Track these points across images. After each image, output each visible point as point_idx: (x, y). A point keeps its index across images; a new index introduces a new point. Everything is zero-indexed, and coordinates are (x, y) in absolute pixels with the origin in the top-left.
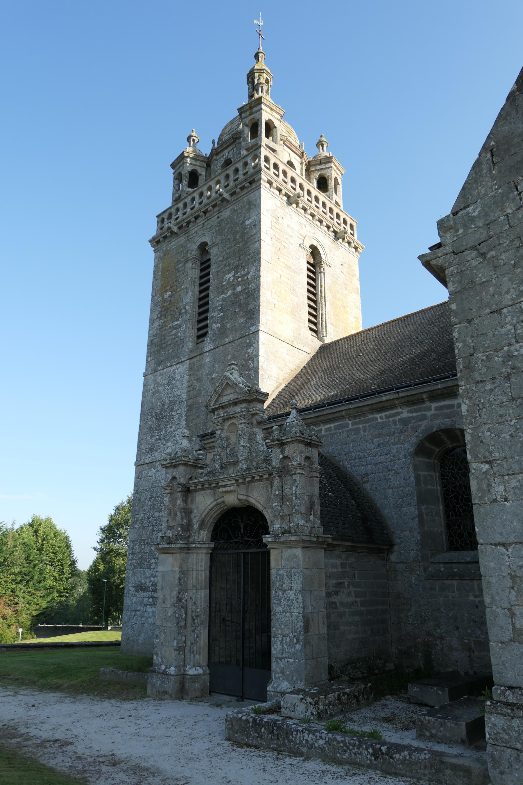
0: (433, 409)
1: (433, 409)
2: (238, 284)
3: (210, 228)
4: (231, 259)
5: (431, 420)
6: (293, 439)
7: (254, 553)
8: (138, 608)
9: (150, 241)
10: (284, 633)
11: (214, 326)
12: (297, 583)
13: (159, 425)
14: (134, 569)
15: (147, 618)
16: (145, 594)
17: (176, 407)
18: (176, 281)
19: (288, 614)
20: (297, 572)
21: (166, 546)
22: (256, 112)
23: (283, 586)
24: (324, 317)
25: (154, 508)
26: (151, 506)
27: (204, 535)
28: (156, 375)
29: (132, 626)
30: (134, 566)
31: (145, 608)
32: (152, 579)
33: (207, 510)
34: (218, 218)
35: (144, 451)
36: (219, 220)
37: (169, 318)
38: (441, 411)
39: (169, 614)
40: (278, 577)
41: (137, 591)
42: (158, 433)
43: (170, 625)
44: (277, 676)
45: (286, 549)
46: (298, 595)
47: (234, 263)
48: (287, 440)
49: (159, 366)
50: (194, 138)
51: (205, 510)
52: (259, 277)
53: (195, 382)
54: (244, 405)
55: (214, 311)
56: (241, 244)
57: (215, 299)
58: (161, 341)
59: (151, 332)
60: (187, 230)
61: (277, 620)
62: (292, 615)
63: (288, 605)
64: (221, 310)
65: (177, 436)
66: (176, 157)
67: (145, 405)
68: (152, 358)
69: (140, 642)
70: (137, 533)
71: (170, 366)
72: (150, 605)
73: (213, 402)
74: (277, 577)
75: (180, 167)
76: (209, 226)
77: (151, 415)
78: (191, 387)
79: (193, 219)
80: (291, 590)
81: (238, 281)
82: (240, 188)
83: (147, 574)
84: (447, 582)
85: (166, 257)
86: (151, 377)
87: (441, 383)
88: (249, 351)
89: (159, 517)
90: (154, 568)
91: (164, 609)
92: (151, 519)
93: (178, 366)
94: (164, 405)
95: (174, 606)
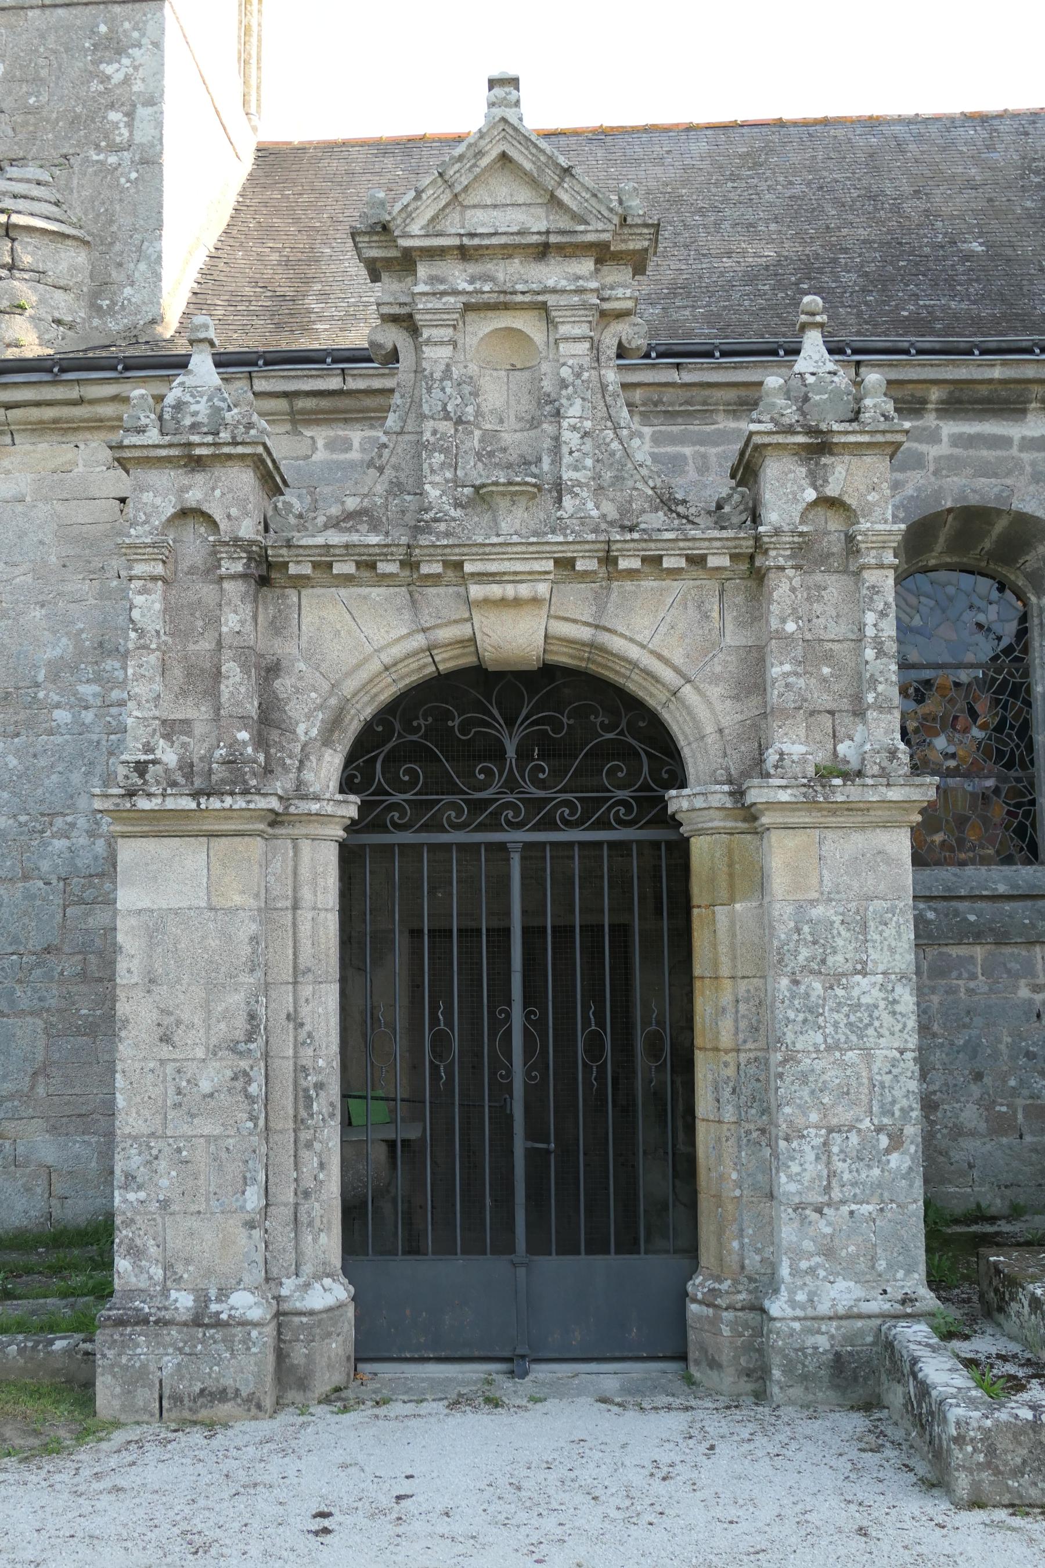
0: (945, 439)
1: (945, 439)
5: (935, 473)
6: (880, 438)
7: (570, 845)
10: (835, 1121)
12: (892, 950)
19: (851, 1056)
20: (892, 910)
23: (830, 960)
24: (254, 40)
27: (327, 768)
33: (375, 666)
38: (972, 452)
39: (206, 1086)
40: (806, 929)
44: (804, 1265)
45: (840, 833)
46: (899, 989)
48: (852, 439)
51: (358, 666)
54: (587, 266)
61: (804, 1078)
62: (868, 1056)
63: (849, 1025)
73: (423, 221)
74: (798, 931)
80: (864, 973)
84: (954, 951)
87: (1004, 363)
88: (109, 69)
91: (170, 1068)
95: (233, 1050)
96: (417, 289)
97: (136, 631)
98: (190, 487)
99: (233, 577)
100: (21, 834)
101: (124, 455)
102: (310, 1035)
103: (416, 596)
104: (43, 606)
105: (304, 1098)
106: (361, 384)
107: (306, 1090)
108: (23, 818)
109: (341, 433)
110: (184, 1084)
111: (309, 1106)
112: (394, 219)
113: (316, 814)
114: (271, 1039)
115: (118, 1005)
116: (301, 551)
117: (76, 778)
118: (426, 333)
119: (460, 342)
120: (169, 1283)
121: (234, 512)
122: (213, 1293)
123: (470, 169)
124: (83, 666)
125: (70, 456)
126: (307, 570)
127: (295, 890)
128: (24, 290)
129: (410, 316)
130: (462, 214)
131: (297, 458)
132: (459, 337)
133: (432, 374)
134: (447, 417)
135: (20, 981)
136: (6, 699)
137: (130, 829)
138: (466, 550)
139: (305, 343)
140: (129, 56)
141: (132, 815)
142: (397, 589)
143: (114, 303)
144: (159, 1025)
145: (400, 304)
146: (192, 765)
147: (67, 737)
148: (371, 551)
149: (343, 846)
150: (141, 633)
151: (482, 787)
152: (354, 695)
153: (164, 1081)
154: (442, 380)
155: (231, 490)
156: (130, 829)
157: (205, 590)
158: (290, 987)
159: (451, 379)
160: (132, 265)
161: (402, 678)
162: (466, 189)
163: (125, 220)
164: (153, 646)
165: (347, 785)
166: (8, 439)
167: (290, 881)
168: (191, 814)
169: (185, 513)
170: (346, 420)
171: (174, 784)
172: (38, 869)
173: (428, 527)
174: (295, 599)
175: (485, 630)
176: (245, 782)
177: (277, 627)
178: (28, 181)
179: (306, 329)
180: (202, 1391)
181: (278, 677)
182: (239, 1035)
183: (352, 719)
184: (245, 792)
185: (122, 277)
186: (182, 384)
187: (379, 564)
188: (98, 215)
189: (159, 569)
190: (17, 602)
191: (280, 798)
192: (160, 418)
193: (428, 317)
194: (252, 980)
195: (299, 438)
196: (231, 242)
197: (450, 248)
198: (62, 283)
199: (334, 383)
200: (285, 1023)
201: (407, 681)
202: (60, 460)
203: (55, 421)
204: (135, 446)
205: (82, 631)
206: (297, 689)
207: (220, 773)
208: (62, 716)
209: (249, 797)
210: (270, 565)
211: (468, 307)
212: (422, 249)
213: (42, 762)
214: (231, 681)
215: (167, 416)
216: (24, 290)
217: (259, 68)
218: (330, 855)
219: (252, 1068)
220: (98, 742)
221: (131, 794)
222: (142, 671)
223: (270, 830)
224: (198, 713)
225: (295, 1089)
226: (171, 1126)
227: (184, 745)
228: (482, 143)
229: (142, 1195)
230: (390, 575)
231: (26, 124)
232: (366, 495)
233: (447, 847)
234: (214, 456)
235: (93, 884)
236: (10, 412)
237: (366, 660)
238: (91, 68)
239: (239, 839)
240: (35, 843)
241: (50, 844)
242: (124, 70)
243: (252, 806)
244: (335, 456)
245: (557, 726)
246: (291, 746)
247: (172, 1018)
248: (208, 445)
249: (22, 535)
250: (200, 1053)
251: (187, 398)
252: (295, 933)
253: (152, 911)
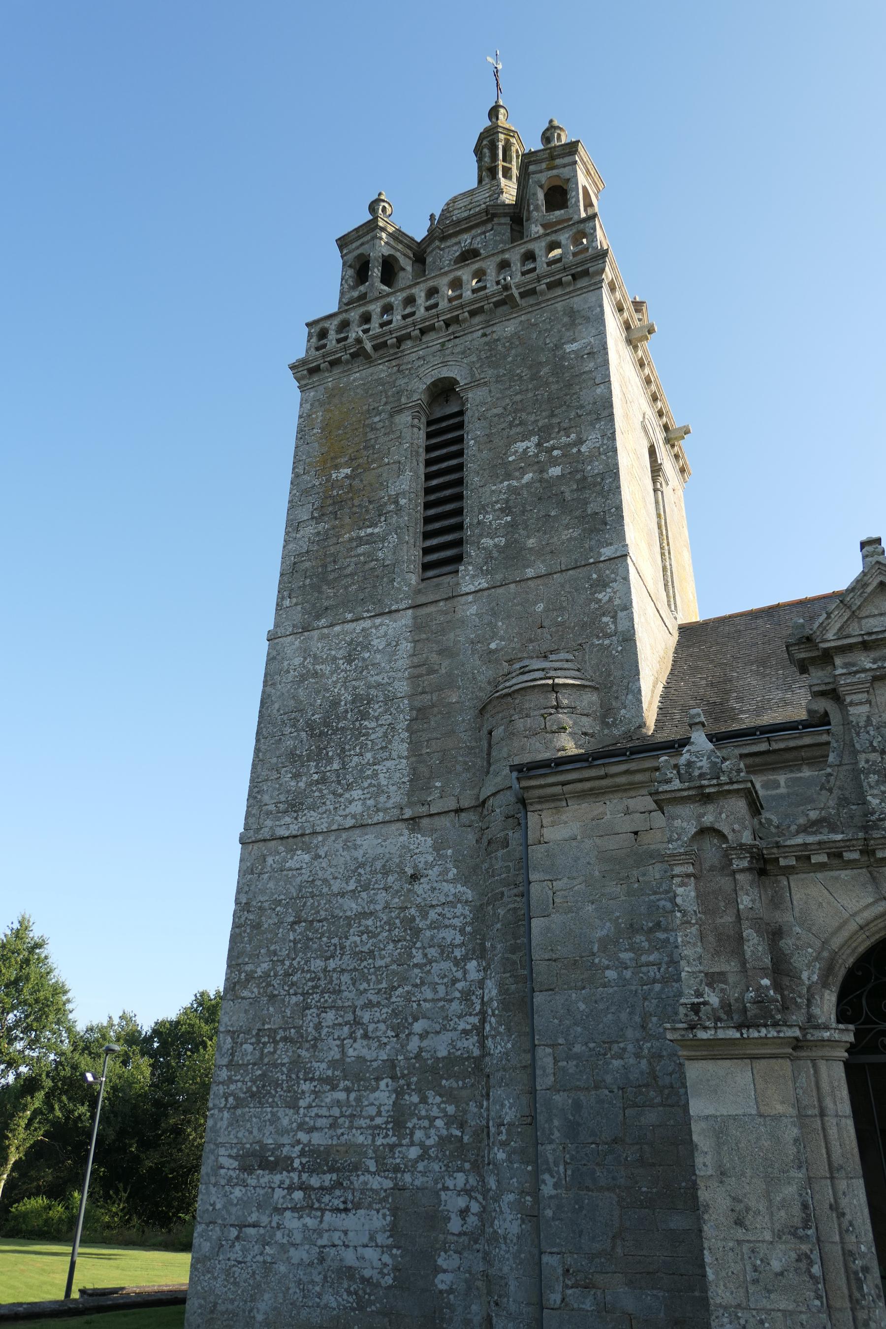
2: (554, 462)
3: (463, 353)
4: (528, 414)
8: (253, 1218)
9: (292, 367)
11: (487, 542)
13: (320, 750)
14: (235, 1108)
15: (283, 1248)
16: (277, 1178)
17: (376, 709)
18: (366, 448)
21: (734, 1034)
22: (564, 166)
24: (669, 573)
25: (307, 947)
26: (295, 942)
27: (827, 1005)
28: (310, 638)
29: (228, 1272)
30: (237, 1098)
31: (276, 1219)
32: (302, 1136)
33: (853, 926)
34: (484, 335)
35: (272, 808)
36: (485, 339)
37: (347, 520)
41: (246, 1168)
42: (316, 767)
43: (784, 1304)
47: (536, 421)
49: (318, 617)
50: (387, 205)
51: (840, 928)
52: (615, 450)
53: (434, 658)
55: (483, 509)
56: (554, 387)
57: (486, 488)
58: (324, 566)
59: (291, 546)
60: (396, 353)
64: (506, 510)
65: (381, 776)
66: (356, 226)
67: (273, 702)
68: (294, 600)
69: (260, 1317)
70: (246, 1011)
71: (352, 621)
72: (294, 1209)
75: (362, 244)
76: (457, 350)
77: (294, 726)
78: (420, 670)
79: (417, 332)
81: (551, 457)
82: (547, 284)
83: (285, 1122)
85: (336, 401)
86: (292, 645)
88: (600, 596)
89: (325, 970)
90: (310, 1106)
91: (745, 1248)
92: (299, 975)
93: (378, 621)
94: (335, 704)
95: (794, 1235)
96: (839, 671)
97: (680, 912)
98: (705, 814)
99: (742, 871)
100: (591, 1056)
101: (660, 798)
102: (851, 1224)
103: (875, 874)
104: (593, 903)
105: (855, 1280)
106: (782, 745)
107: (856, 1273)
108: (592, 1045)
109: (771, 777)
110: (758, 1262)
111: (860, 1289)
112: (815, 632)
113: (828, 1040)
114: (819, 1225)
115: (699, 1192)
116: (787, 849)
117: (624, 1016)
118: (848, 699)
119: (873, 701)
121: (736, 827)
123: (860, 595)
124: (621, 940)
125: (601, 809)
126: (793, 862)
127: (820, 1100)
128: (565, 719)
129: (834, 690)
130: (859, 622)
132: (872, 697)
133: (858, 724)
134: (874, 750)
135: (598, 1164)
136: (575, 964)
137: (693, 1053)
139: (735, 727)
140: (610, 587)
141: (694, 1043)
142: (860, 871)
143: (615, 720)
144: (732, 1210)
145: (826, 684)
146: (730, 1005)
147: (615, 988)
148: (838, 845)
149: (847, 1065)
150: (684, 913)
152: (840, 949)
153: (742, 1259)
154: (866, 727)
155: (732, 813)
156: (693, 1053)
157: (723, 881)
158: (829, 1181)
159: (872, 725)
160: (624, 697)
161: (873, 934)
162: (859, 607)
163: (618, 673)
164: (693, 921)
165: (842, 1018)
166: (564, 804)
167: (814, 1093)
168: (736, 1042)
169: (704, 832)
170: (774, 769)
171: (719, 1019)
172: (604, 1081)
173: (876, 825)
174: (786, 883)
176: (772, 1017)
177: (776, 903)
178: (562, 661)
179: (734, 719)
181: (782, 938)
182: (797, 1221)
183: (840, 967)
184: (775, 1024)
185: (619, 704)
186: (688, 751)
187: (844, 854)
188: (602, 672)
189: (690, 869)
190: (577, 902)
191: (800, 1028)
192: (678, 772)
193: (848, 688)
194: (800, 1175)
196: (675, 678)
197: (855, 644)
198: (585, 712)
199: (763, 747)
200: (829, 1212)
201: (877, 936)
202: (596, 813)
203: (591, 789)
204: (666, 792)
205: (618, 917)
206: (797, 946)
207: (752, 1009)
208: (611, 974)
209: (778, 1028)
210: (766, 861)
211: (875, 679)
212: (836, 648)
213: (601, 1006)
214: (751, 943)
215: (682, 772)
216: (565, 719)
217: (673, 587)
218: (839, 1071)
219: (811, 1251)
220: (636, 991)
221: (692, 1027)
222: (688, 939)
223: (795, 1054)
224: (730, 967)
225: (846, 1271)
226: (752, 1299)
227: (722, 990)
228: (866, 578)
230: (855, 860)
231: (558, 631)
232: (822, 809)
234: (719, 793)
235: (675, 1098)
236: (565, 788)
237: (845, 922)
238: (590, 597)
239: (774, 1061)
240: (601, 1063)
241: (611, 1063)
242: (608, 595)
243: (782, 1035)
246: (799, 988)
247: (742, 1205)
248: (714, 785)
249: (576, 860)
250: (768, 1236)
251: (694, 759)
252: (825, 1136)
253: (716, 1117)
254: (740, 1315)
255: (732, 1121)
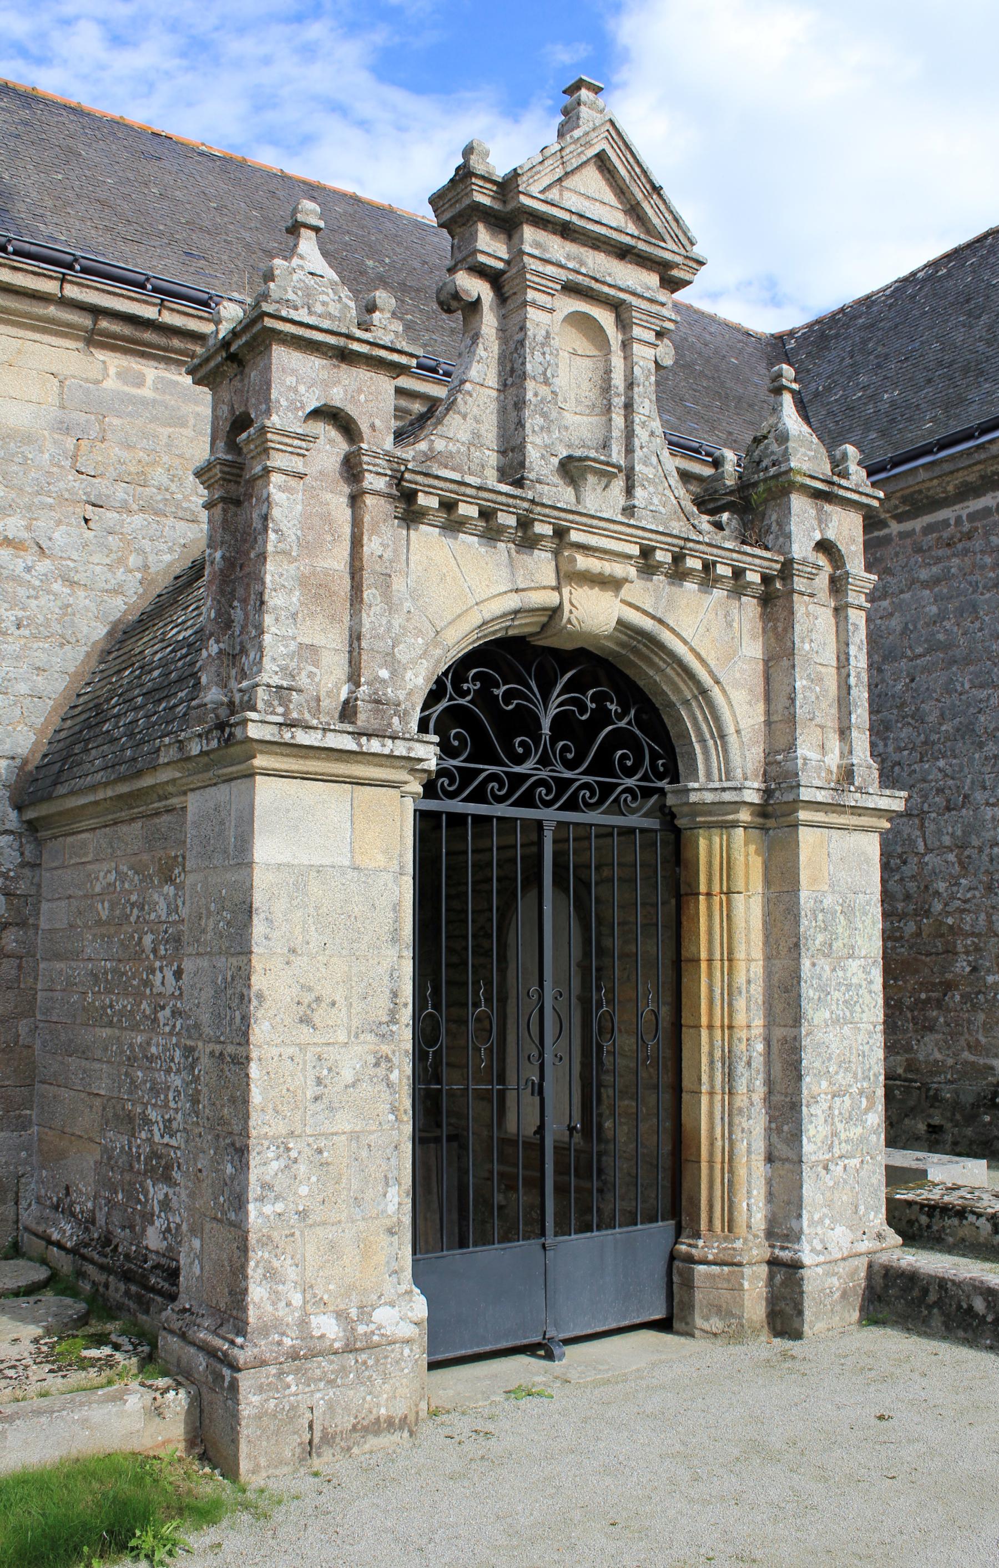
40: (820, 917)
110: (325, 1072)
115: (253, 979)
120: (308, 1307)
122: (354, 1313)
131: (87, 380)
138: (577, 518)
151: (520, 760)
154: (543, 345)
170: (143, 355)
175: (574, 601)
180: (354, 1426)
195: (90, 359)
199: (149, 312)
219: (394, 1052)
229: (279, 1207)
233: (488, 819)
244: (127, 389)
245: (583, 709)
250: (342, 1038)
254: (291, 1145)
255: (315, 874)
